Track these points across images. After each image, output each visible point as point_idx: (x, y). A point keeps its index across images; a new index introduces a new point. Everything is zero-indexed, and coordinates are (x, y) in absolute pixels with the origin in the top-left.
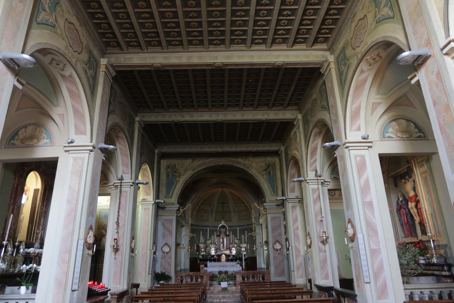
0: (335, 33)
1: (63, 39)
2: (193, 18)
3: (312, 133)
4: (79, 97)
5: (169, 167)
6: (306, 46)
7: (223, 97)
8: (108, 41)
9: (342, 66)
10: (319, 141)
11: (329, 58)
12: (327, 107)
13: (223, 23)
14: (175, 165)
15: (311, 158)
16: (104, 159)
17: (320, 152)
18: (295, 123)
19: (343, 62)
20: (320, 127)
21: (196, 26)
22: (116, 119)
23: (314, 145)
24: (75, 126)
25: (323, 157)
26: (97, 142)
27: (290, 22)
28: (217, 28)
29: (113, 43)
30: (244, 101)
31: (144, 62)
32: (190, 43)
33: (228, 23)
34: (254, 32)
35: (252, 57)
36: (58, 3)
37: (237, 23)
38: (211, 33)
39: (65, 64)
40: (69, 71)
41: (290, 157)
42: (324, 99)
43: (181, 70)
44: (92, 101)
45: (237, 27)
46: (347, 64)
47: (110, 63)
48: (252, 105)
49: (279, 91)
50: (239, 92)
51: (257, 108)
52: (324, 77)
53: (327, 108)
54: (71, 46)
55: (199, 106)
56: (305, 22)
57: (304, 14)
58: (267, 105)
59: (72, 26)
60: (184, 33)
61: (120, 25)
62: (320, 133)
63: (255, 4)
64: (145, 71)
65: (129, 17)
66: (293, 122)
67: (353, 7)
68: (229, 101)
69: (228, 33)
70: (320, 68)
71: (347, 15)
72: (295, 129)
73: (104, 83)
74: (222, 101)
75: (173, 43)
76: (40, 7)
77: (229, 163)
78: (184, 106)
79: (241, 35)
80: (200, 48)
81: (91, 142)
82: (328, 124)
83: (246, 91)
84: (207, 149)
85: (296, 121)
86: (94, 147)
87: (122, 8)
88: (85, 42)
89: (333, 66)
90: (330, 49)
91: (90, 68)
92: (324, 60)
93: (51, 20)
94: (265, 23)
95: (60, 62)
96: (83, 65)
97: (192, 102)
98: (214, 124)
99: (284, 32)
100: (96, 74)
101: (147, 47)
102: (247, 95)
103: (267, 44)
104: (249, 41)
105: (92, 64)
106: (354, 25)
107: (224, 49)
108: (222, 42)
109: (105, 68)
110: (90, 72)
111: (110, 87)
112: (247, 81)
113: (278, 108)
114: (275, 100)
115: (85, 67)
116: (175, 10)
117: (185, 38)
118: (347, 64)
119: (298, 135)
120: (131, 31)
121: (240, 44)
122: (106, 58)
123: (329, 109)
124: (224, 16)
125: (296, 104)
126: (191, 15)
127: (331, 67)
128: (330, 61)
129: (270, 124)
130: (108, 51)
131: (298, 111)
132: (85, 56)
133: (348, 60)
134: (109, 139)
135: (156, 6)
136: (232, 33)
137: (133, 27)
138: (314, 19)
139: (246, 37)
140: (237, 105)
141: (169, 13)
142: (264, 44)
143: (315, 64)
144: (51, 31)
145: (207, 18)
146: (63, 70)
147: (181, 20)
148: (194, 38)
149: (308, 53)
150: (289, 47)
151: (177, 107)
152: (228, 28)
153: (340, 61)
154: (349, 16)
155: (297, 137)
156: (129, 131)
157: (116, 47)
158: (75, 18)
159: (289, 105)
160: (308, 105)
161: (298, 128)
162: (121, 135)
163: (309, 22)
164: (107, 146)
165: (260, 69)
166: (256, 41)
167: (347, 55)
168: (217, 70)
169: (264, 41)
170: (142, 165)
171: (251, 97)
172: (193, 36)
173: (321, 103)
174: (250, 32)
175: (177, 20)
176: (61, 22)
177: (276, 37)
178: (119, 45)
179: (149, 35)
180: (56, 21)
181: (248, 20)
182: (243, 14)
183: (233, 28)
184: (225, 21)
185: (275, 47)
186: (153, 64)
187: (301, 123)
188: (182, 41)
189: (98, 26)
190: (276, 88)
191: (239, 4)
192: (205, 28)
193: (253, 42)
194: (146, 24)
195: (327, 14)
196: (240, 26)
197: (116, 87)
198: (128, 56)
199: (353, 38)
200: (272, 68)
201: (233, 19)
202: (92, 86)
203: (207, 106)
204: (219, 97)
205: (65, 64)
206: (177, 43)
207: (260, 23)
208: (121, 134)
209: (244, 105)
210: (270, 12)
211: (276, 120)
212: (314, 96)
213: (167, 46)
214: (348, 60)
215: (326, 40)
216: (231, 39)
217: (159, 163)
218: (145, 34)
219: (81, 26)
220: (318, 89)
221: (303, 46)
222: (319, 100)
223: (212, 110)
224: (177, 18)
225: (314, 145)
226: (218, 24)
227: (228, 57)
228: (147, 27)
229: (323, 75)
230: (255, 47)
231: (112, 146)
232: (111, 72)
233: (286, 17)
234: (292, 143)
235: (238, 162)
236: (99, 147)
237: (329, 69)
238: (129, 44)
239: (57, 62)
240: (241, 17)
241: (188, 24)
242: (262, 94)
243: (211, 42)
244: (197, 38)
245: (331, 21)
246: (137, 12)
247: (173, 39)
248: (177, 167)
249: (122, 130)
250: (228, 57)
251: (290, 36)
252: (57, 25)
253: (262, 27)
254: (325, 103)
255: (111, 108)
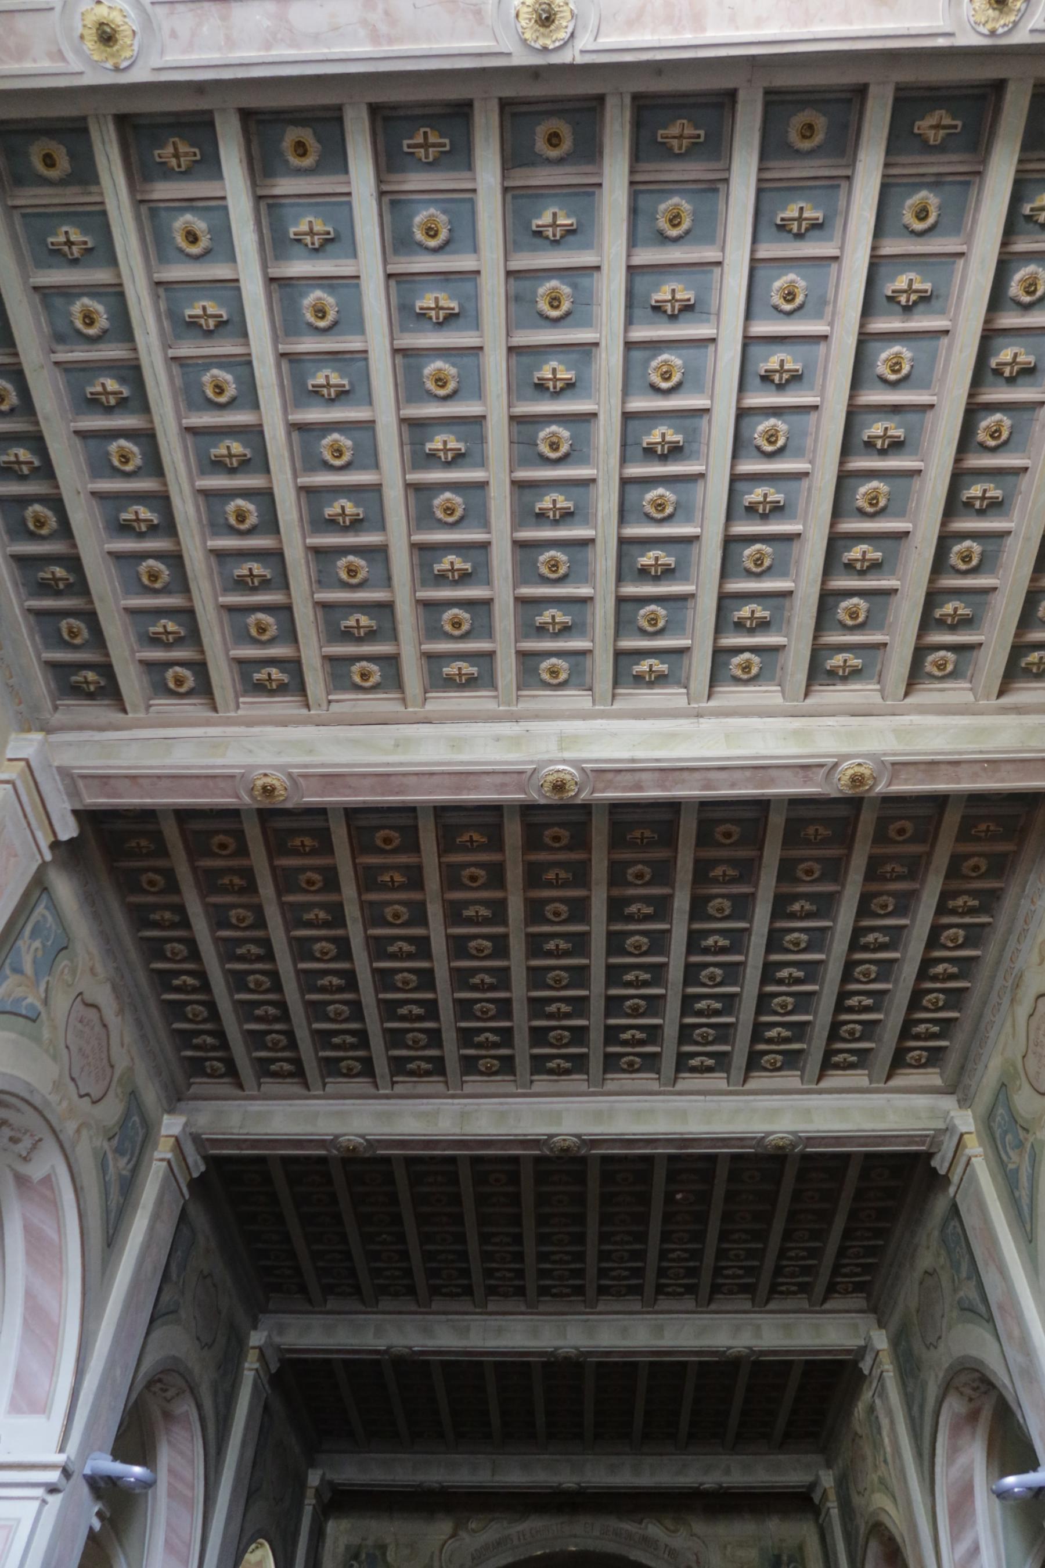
0: (961, 1036)
1: (55, 1058)
2: (484, 991)
3: (942, 1419)
4: (60, 1256)
5: (356, 1557)
6: (869, 1076)
7: (580, 1257)
8: (198, 1057)
9: (1011, 1153)
10: (975, 1455)
11: (957, 1122)
12: (982, 1309)
13: (580, 1005)
14: (383, 1548)
15: (955, 1538)
16: (97, 1525)
17: (984, 1510)
18: (865, 1366)
19: (1009, 1137)
20: (968, 1391)
21: (490, 1014)
22: (177, 1342)
23: (955, 1471)
24: (18, 1376)
25: (1005, 1527)
26: (86, 1449)
27: (805, 1001)
28: (559, 1019)
29: (215, 1063)
30: (661, 1272)
31: (309, 1129)
32: (469, 1066)
33: (597, 1006)
34: (685, 1033)
35: (683, 1114)
36: (66, 948)
37: (629, 1003)
38: (538, 1036)
39: (40, 1140)
40: (49, 1163)
41: (863, 1530)
42: (964, 1274)
43: (432, 1158)
44: (103, 1273)
45: (628, 1016)
46: (1028, 1146)
47: (193, 1130)
48: (691, 1290)
49: (787, 1235)
50: (642, 1237)
51: (710, 1301)
52: (952, 1190)
53: (980, 1311)
54: (73, 1079)
55: (492, 1291)
56: (853, 1001)
57: (847, 975)
58: (748, 1289)
59: (92, 1014)
60: (449, 1037)
61: (246, 1010)
62: (973, 1417)
63: (684, 949)
64: (307, 1158)
65: (277, 986)
66: (855, 1363)
67: (1008, 954)
68: (602, 1273)
69: (596, 1036)
70: (930, 1155)
71: (993, 977)
72: (867, 1395)
73: (159, 1202)
74: (580, 1273)
75: (411, 1066)
76: (8, 961)
77: (611, 1547)
78: (435, 1291)
79: (642, 1043)
80: (501, 1083)
81: (62, 1450)
82: (998, 1384)
83: (665, 1237)
84: (516, 1474)
85: (868, 1360)
86: (66, 1473)
87: (259, 959)
88: (122, 1063)
89: (974, 1148)
90: (957, 1087)
91: (119, 1151)
92: (941, 1125)
93: (29, 1000)
94: (718, 1006)
95: (25, 1133)
96: (101, 1142)
97: (466, 1273)
98: (545, 1364)
99: (786, 1033)
100: (135, 1170)
101: (323, 1077)
102: (674, 1250)
103: (733, 1072)
104: (668, 1063)
105: (132, 1137)
106: (1022, 1011)
107: (584, 1087)
108: (579, 1064)
109: (172, 1150)
110: (120, 1165)
111: (177, 1213)
112: (669, 1198)
113: (790, 1303)
114: (778, 1271)
115: (106, 1145)
116: (425, 964)
117: (451, 1050)
118: (1028, 1146)
119: (885, 1422)
120: (278, 1027)
121: (637, 1071)
122: (181, 1113)
123: (990, 1319)
124: (584, 984)
125: (859, 1288)
126: (476, 980)
127: (968, 1151)
128: (963, 1129)
129: (766, 1372)
130: (193, 1090)
131: (872, 1318)
132: (111, 1111)
133: (1027, 1130)
134: (134, 1438)
135: (366, 954)
136: (611, 1034)
137: (285, 1015)
138: (884, 992)
139: (658, 1049)
140: (636, 1290)
141: (406, 974)
142: (722, 1071)
143: (910, 1139)
144: (22, 1034)
145: (528, 990)
146: (26, 1159)
147: (444, 995)
148: (483, 1052)
149: (878, 1100)
150: (810, 1082)
151: (411, 1291)
152: (596, 1021)
153: (998, 1133)
154: (999, 982)
155: (880, 1433)
156: (215, 1395)
157: (221, 1076)
158: (108, 988)
159: (831, 1290)
160: (908, 1296)
161: (882, 1392)
162: (185, 1408)
163: (868, 1002)
164: (118, 1468)
165: (712, 1159)
166: (694, 1062)
167: (1023, 1114)
168: (558, 1158)
169: (722, 1062)
170: (245, 1551)
171: (686, 1260)
172: (479, 1046)
173: (955, 1290)
174: (671, 1032)
175: (430, 996)
176: (62, 1002)
177: (785, 1263)
178: (232, 1071)
179: (336, 1040)
180: (46, 1002)
181: (663, 997)
182: (645, 976)
183: (612, 1021)
184: (586, 998)
185: (759, 1081)
186: (337, 1136)
187: (888, 1368)
188: (441, 1059)
189: (174, 1010)
190: (778, 1226)
191: (632, 950)
192: (521, 1020)
193: (683, 1064)
194: (331, 1008)
195: (923, 974)
196: (636, 1012)
197: (200, 1219)
198: (256, 1106)
199: (1030, 1055)
200: (755, 1155)
201: (613, 992)
202: (113, 1215)
203: (520, 1292)
204: (566, 1258)
205: (40, 1140)
206: (424, 1066)
207: (702, 1005)
208: (186, 1407)
209: (660, 1290)
210: (733, 973)
211: (788, 1352)
212: (926, 1260)
213: (392, 1076)
214: (1027, 1130)
215: (935, 1058)
216: (607, 1056)
217: (318, 1535)
218: (323, 1038)
219: (121, 1011)
220: (936, 1233)
221: (859, 1078)
222: (945, 1279)
223: (542, 1308)
224: (433, 988)
225: (955, 1471)
226: (565, 1008)
227: (598, 1116)
228: (332, 1015)
229: (946, 1180)
230: (689, 1082)
231: (137, 1470)
232: (190, 1161)
233: (789, 985)
234: (864, 1458)
235: (647, 1541)
236: (87, 1471)
237: (963, 1161)
238: (264, 1069)
239: (12, 1134)
240: (637, 987)
241: (464, 1009)
242: (726, 1246)
243: (539, 1065)
244: (493, 1052)
245: (941, 996)
246: (305, 972)
247: (412, 1053)
248: (390, 1557)
249: (193, 1391)
250: (598, 1116)
251: (809, 1045)
252: (44, 1015)
253: (708, 1016)
254: (969, 1292)
255: (165, 1297)
